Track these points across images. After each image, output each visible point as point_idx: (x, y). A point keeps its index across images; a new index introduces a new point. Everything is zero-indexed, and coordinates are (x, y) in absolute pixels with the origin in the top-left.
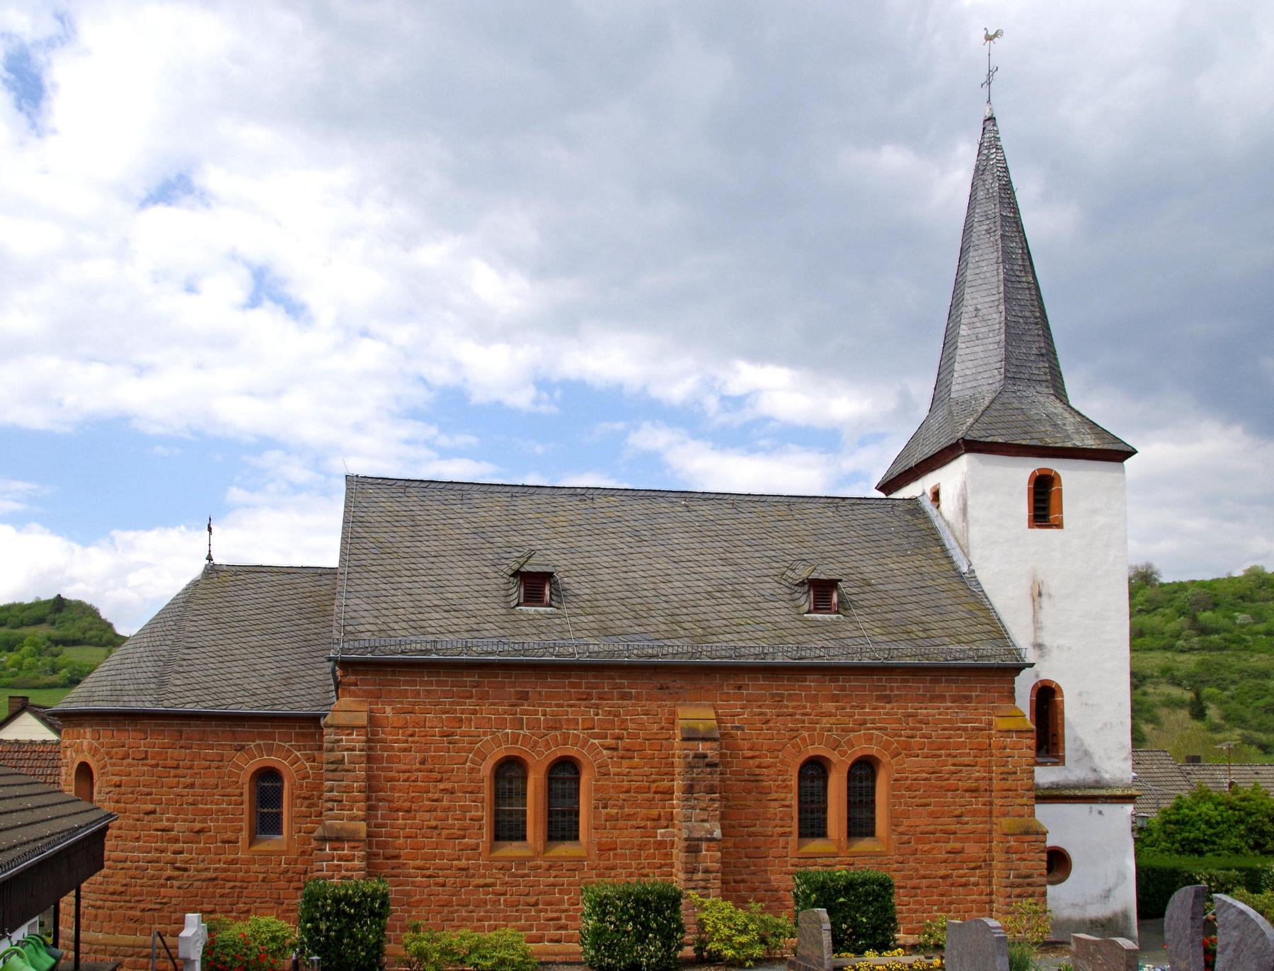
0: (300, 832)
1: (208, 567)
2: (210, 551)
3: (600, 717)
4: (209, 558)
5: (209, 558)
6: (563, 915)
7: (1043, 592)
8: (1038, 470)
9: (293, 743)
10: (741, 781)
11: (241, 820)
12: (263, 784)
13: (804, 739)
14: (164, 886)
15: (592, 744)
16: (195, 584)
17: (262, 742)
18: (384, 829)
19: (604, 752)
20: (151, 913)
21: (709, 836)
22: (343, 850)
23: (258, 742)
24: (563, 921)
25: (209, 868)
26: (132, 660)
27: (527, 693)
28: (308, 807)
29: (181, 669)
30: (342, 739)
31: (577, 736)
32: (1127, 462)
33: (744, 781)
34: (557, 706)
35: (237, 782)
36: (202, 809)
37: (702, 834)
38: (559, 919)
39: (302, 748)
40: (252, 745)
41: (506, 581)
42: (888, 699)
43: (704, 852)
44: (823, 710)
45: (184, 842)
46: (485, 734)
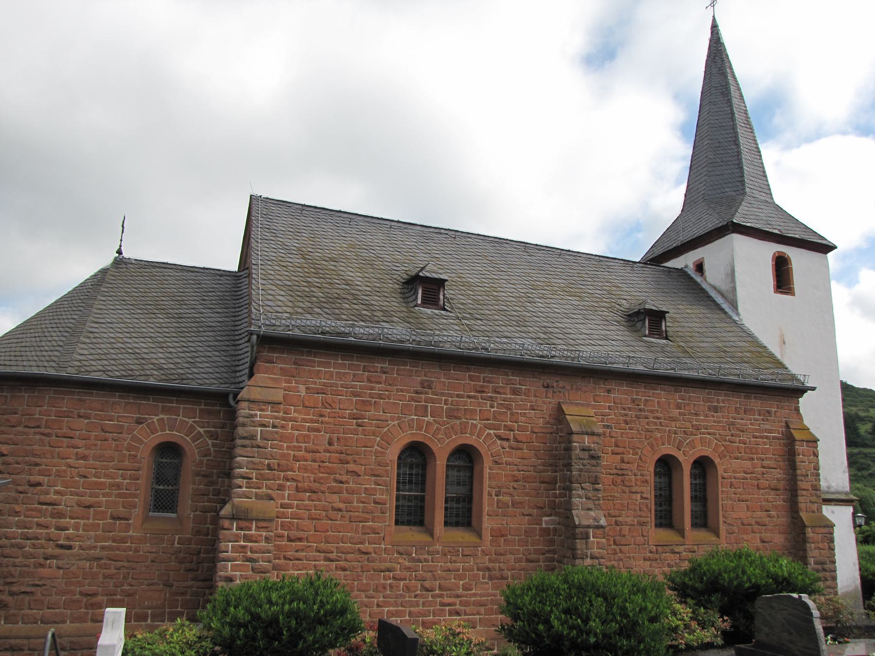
0: (196, 510)
1: (118, 259)
2: (120, 246)
3: (495, 409)
4: (119, 252)
5: (119, 252)
6: (458, 601)
7: (786, 341)
8: (777, 252)
9: (197, 419)
10: (610, 474)
11: (136, 496)
12: (161, 460)
13: (656, 439)
14: (42, 566)
15: (489, 434)
16: (104, 272)
17: (165, 417)
18: (290, 510)
19: (499, 442)
20: (22, 596)
21: (596, 524)
22: (250, 529)
23: (162, 416)
24: (458, 606)
25: (95, 547)
26: (36, 330)
27: (433, 382)
28: (206, 485)
29: (88, 341)
30: (256, 415)
31: (475, 426)
32: (830, 255)
33: (613, 474)
34: (458, 396)
35: (136, 456)
36: (96, 482)
37: (591, 522)
38: (454, 604)
39: (206, 425)
40: (155, 418)
41: (401, 287)
42: (716, 409)
43: (592, 539)
44: (671, 415)
45: (71, 518)
46: (393, 419)
